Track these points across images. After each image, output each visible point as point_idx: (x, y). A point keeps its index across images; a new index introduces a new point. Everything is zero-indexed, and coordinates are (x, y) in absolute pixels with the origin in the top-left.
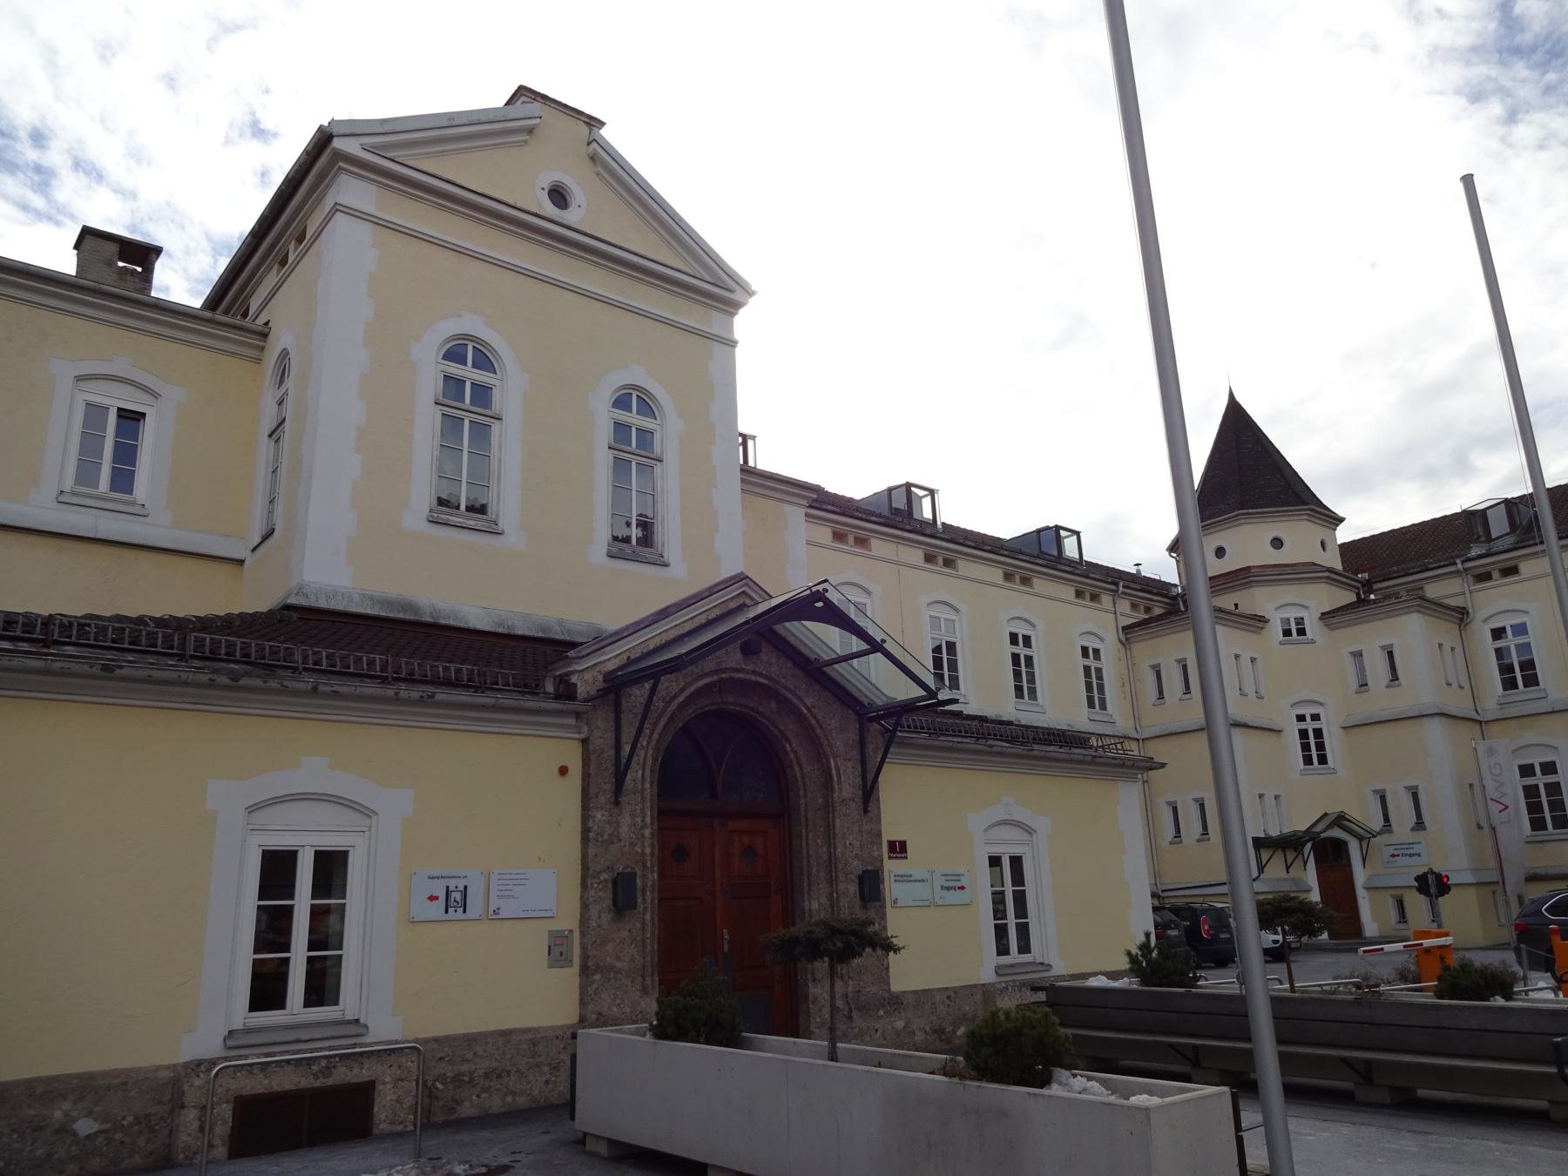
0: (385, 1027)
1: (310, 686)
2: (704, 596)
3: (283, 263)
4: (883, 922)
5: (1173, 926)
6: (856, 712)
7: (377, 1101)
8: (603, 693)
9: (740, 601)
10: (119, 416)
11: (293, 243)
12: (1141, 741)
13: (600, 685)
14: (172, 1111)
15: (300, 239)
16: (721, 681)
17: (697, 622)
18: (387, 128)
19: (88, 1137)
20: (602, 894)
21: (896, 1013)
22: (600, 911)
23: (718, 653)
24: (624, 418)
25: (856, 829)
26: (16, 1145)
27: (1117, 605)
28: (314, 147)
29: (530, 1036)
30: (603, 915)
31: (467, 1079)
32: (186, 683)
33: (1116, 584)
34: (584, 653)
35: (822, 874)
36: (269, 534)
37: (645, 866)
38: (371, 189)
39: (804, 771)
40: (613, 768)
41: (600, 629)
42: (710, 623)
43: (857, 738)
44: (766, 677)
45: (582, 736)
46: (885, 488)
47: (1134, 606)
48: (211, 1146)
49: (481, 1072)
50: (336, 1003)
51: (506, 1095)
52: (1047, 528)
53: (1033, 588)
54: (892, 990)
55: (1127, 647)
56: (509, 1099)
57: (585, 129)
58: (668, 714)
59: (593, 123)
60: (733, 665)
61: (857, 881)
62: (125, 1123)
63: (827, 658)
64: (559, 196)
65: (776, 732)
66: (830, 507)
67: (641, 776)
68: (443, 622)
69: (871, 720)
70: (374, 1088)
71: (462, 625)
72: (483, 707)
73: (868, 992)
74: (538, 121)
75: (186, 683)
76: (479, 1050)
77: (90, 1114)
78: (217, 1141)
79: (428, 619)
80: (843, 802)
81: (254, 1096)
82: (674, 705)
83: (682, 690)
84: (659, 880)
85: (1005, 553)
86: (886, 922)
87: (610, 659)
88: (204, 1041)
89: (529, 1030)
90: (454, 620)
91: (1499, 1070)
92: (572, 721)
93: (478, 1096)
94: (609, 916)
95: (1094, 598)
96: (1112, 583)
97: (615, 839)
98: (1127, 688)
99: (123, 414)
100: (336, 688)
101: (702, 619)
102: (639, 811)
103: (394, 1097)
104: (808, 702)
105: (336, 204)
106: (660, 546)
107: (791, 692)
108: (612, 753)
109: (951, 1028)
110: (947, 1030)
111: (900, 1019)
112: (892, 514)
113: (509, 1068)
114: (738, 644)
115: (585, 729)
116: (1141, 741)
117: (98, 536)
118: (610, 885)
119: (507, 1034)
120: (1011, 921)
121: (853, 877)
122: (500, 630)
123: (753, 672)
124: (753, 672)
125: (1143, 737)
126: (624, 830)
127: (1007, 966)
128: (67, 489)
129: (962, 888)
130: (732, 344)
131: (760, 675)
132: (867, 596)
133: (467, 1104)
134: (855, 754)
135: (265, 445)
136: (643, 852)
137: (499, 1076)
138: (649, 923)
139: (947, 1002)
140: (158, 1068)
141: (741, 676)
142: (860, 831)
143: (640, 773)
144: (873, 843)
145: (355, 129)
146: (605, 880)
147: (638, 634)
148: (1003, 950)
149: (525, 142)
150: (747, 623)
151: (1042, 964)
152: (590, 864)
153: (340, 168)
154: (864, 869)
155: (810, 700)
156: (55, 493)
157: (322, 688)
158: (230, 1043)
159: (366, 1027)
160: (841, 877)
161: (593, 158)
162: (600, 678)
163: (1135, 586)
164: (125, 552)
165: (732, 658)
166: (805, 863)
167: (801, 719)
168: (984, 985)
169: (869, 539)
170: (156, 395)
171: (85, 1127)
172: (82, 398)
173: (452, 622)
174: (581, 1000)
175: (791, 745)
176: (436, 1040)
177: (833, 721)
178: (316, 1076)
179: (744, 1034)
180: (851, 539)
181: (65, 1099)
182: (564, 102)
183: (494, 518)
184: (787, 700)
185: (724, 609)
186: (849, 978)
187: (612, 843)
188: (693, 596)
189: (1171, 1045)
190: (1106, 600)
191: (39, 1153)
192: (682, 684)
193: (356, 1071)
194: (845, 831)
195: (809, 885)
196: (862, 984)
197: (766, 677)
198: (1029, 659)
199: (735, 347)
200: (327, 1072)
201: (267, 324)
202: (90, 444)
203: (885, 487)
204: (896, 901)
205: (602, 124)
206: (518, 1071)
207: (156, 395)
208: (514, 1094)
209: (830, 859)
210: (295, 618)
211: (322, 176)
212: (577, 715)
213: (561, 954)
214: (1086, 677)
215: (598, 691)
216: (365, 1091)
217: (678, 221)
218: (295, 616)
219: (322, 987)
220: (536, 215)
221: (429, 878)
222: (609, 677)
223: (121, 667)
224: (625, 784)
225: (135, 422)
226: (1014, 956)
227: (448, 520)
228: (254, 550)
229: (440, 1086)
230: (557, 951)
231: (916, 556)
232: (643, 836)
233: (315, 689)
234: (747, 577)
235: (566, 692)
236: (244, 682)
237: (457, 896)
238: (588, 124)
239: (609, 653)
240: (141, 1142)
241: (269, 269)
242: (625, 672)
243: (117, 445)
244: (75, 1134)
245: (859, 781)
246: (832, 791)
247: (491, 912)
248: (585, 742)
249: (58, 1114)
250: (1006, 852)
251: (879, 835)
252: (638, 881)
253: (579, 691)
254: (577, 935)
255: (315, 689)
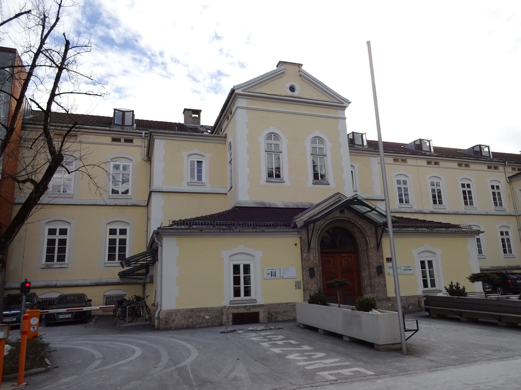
0: (261, 301)
1: (238, 231)
2: (328, 199)
3: (228, 119)
4: (384, 279)
5: (519, 279)
6: (374, 225)
7: (260, 316)
8: (304, 226)
9: (339, 199)
10: (197, 162)
11: (230, 114)
12: (517, 216)
13: (303, 224)
14: (221, 315)
15: (231, 113)
16: (335, 220)
17: (327, 206)
18: (247, 84)
19: (208, 319)
20: (307, 273)
21: (389, 302)
22: (306, 277)
23: (333, 213)
24: (315, 146)
25: (375, 255)
26: (196, 320)
27: (505, 170)
28: (231, 93)
29: (292, 304)
30: (307, 278)
31: (279, 312)
32: (215, 232)
33: (505, 162)
34: (298, 217)
35: (367, 267)
36: (231, 188)
37: (317, 266)
38: (245, 100)
39: (360, 240)
40: (307, 243)
41: (312, 204)
42: (331, 206)
43: (374, 231)
44: (347, 218)
45: (300, 236)
46: (413, 141)
47: (513, 169)
48: (229, 322)
49: (282, 311)
50: (250, 296)
51: (288, 316)
52: (477, 145)
53: (470, 168)
54: (388, 296)
55: (510, 184)
56: (288, 317)
57: (298, 68)
58: (321, 229)
59: (300, 65)
60: (337, 216)
61: (376, 268)
62: (214, 317)
63: (365, 211)
64: (292, 89)
65: (352, 231)
66: (392, 152)
67: (314, 244)
68: (271, 206)
69: (379, 226)
70: (259, 313)
71: (276, 207)
72: (275, 232)
73: (381, 297)
74: (285, 70)
75: (215, 232)
76: (281, 307)
77: (207, 315)
78: (230, 322)
79: (268, 206)
80: (371, 248)
81: (236, 313)
82: (322, 227)
83: (324, 223)
84: (322, 269)
85: (458, 157)
86: (385, 279)
87: (305, 218)
88: (226, 303)
89: (292, 303)
90: (274, 205)
91: (447, 310)
92: (297, 233)
93: (282, 316)
94: (309, 278)
95: (496, 168)
96: (503, 162)
97: (309, 260)
98: (511, 198)
99: (198, 162)
100: (244, 231)
101: (329, 205)
102: (315, 254)
103: (263, 315)
104: (360, 223)
105: (237, 106)
106: (327, 179)
107: (354, 221)
108: (307, 240)
109: (407, 307)
110: (406, 307)
111: (390, 304)
112: (416, 149)
113: (288, 311)
114: (339, 210)
115: (300, 235)
116: (517, 216)
117: (197, 192)
118: (309, 271)
119: (287, 303)
120: (429, 279)
121: (375, 268)
122: (286, 207)
123: (344, 217)
124: (344, 217)
125: (518, 214)
126: (311, 258)
127: (427, 291)
128: (189, 182)
129: (411, 270)
130: (345, 118)
131: (345, 217)
132: (407, 178)
133: (279, 318)
134: (374, 236)
135: (228, 164)
136: (316, 263)
137: (286, 312)
138: (319, 279)
139: (406, 300)
140: (218, 307)
141: (340, 218)
142: (377, 256)
143: (314, 245)
144: (381, 259)
145: (239, 87)
146: (307, 270)
147: (312, 211)
148: (425, 285)
149: (282, 76)
150: (335, 207)
151: (439, 290)
152: (303, 266)
153: (237, 97)
154: (378, 265)
155: (360, 223)
156: (186, 183)
157: (241, 231)
158: (231, 303)
159: (257, 301)
160: (371, 267)
161: (300, 75)
162: (303, 222)
163: (513, 162)
164: (202, 195)
165: (337, 214)
166: (362, 264)
167: (358, 228)
168: (418, 296)
169: (406, 160)
170: (204, 156)
171: (207, 317)
172: (189, 160)
173: (274, 206)
174: (304, 297)
175: (356, 234)
176: (272, 304)
177: (367, 228)
178: (246, 311)
179: (327, 303)
180: (400, 160)
181: (203, 312)
182: (291, 62)
183: (282, 178)
184: (354, 223)
185: (334, 202)
186: (375, 293)
187: (308, 261)
188: (325, 200)
189: (451, 310)
190: (501, 168)
191: (200, 321)
192: (324, 222)
193: (255, 310)
194: (372, 256)
195: (363, 270)
196: (378, 294)
197: (347, 218)
198: (470, 192)
199: (346, 119)
200: (249, 309)
201: (226, 134)
202: (192, 170)
203: (413, 141)
204: (389, 274)
205: (302, 65)
206: (290, 311)
207: (204, 156)
208: (289, 316)
209: (368, 263)
210: (238, 210)
211: (234, 99)
212: (298, 232)
213: (298, 286)
214: (493, 196)
215: (303, 225)
216: (257, 314)
217: (326, 87)
218: (238, 209)
219: (247, 293)
220: (286, 96)
221: (149, 295)
222: (305, 222)
223: (203, 230)
224: (311, 247)
225: (200, 163)
226: (430, 288)
227: (271, 181)
228: (229, 191)
229: (273, 314)
230: (297, 285)
231: (424, 163)
232: (316, 259)
233: (239, 231)
234: (340, 193)
235: (295, 227)
236: (225, 231)
237: (274, 273)
238: (299, 66)
239: (304, 217)
240: (217, 321)
241: (225, 120)
242: (309, 220)
243: (198, 169)
244: (205, 318)
245: (375, 243)
246: (368, 245)
247: (281, 277)
248: (300, 237)
249: (202, 315)
250: (426, 260)
251: (382, 256)
252: (315, 269)
253: (298, 226)
254: (302, 282)
255: (239, 231)
